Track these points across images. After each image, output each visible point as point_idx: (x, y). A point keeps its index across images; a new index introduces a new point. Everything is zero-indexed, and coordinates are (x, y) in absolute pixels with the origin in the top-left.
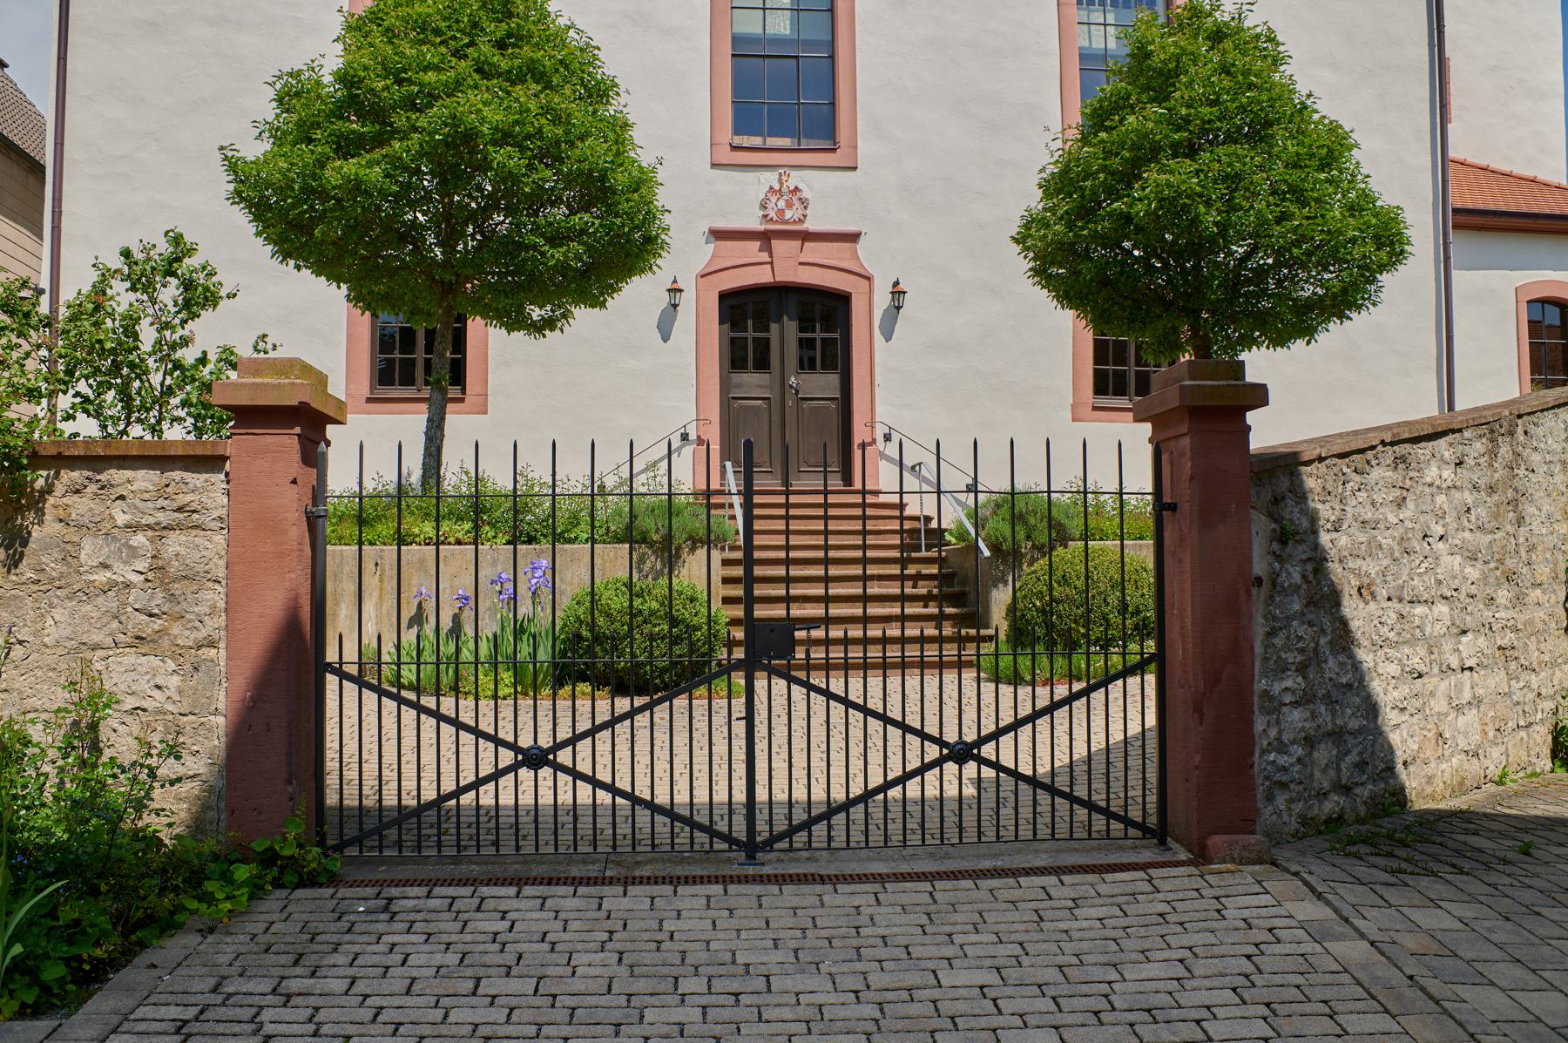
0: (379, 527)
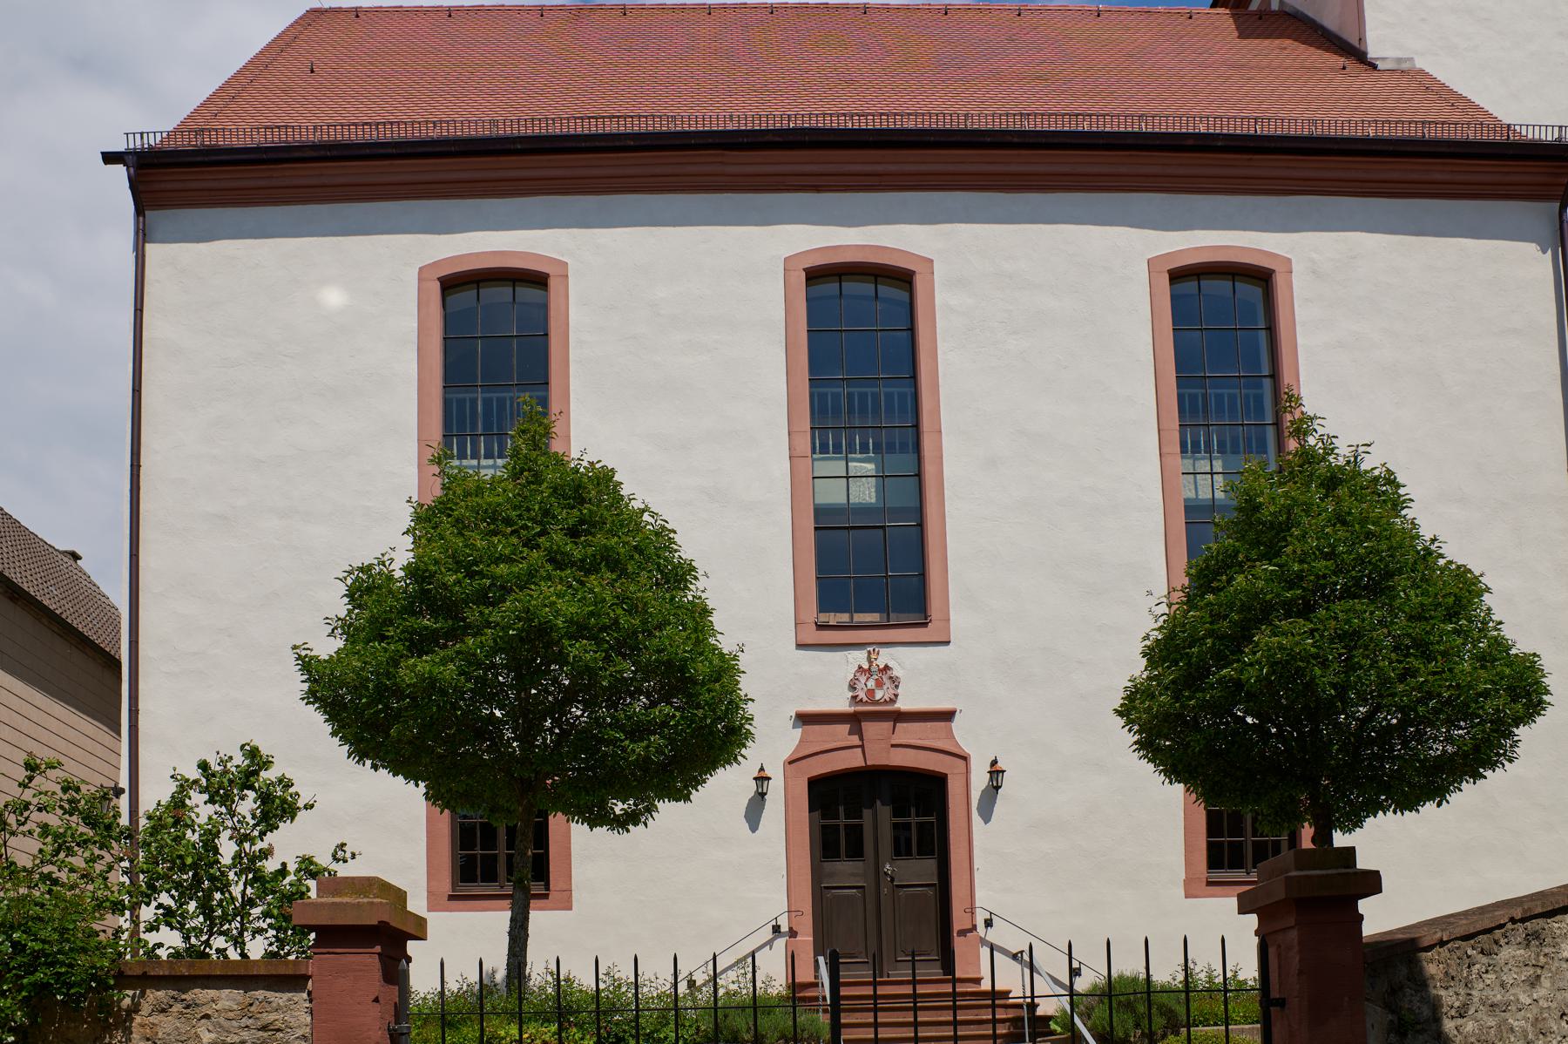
0: (465, 1030)
